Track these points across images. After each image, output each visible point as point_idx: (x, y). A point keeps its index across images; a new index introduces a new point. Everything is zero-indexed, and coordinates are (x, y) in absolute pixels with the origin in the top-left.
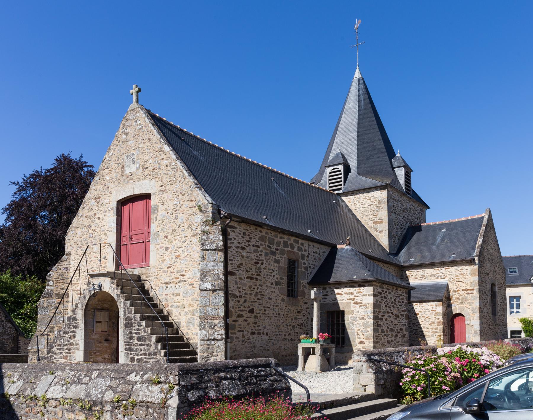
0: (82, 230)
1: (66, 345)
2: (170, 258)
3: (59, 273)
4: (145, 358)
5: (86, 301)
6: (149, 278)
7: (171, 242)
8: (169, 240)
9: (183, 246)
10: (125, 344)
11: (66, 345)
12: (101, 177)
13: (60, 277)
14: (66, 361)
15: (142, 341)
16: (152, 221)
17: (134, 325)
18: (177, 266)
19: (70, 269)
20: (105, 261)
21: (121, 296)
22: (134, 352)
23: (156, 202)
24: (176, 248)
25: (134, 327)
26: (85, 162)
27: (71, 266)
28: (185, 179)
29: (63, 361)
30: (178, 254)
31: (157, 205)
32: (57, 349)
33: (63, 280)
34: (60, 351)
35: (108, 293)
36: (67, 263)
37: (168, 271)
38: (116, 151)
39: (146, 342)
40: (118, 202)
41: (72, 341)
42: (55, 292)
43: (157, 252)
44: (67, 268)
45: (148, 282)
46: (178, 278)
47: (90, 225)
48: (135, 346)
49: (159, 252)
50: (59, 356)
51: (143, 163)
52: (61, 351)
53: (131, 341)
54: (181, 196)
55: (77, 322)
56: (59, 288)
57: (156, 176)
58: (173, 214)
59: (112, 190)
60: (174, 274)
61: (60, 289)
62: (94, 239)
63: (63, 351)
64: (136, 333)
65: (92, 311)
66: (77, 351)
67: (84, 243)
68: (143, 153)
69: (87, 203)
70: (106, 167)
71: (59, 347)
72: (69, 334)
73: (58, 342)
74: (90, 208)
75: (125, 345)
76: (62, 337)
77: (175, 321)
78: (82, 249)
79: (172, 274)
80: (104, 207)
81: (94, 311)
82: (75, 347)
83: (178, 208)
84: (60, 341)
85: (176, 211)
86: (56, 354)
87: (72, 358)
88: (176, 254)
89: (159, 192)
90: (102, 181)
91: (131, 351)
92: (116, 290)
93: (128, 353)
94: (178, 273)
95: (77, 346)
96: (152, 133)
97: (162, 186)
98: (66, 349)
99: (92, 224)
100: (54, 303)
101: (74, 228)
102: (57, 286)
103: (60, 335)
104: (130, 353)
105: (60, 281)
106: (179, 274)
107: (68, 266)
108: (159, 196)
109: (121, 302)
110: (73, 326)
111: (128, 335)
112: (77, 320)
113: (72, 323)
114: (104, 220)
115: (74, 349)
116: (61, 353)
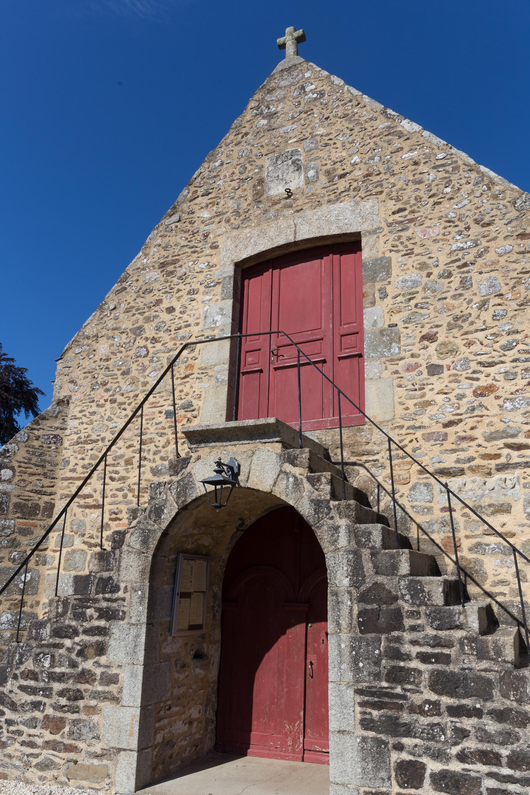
0: (111, 342)
1: (61, 678)
2: (452, 396)
3: (33, 447)
4: (490, 775)
5: (164, 526)
6: (364, 458)
7: (453, 351)
8: (444, 344)
9: (508, 359)
10: (359, 699)
11: (61, 678)
12: (185, 216)
13: (34, 459)
14: (58, 737)
15: (466, 696)
16: (366, 301)
17: (408, 622)
18: (486, 420)
19: (65, 439)
20: (189, 415)
21: (338, 507)
22: (417, 741)
23: (382, 250)
24: (474, 366)
25: (413, 628)
26: (5, 354)
27: (68, 432)
28: (491, 183)
29: (40, 736)
30: (484, 382)
31: (384, 258)
32: (22, 688)
33: (43, 467)
34: (30, 698)
35: (269, 495)
36: (57, 423)
37: (446, 435)
38: (235, 155)
39: (489, 697)
40: (237, 265)
41: (88, 665)
42: (15, 500)
43: (396, 382)
44: (55, 436)
45: (362, 471)
46: (498, 456)
47: (140, 328)
48: (422, 712)
49: (404, 382)
50: (28, 716)
51: (329, 167)
52: (39, 698)
53: (398, 690)
54: (476, 230)
55: (115, 596)
56: (28, 488)
57: (379, 189)
58: (450, 275)
59: (221, 241)
60: (474, 444)
61: (31, 491)
62: (151, 361)
63: (45, 700)
64: (424, 658)
65: (173, 557)
66: (106, 706)
67: (116, 372)
68: (326, 145)
69: (135, 278)
70: (199, 193)
71: (32, 683)
72: (77, 639)
73: (29, 665)
74: (144, 288)
75: (362, 704)
76: (48, 646)
77: (499, 599)
78: (108, 386)
79: (464, 445)
80: (188, 280)
81: (176, 560)
82: (100, 688)
83: (469, 258)
84: (37, 660)
85: (465, 265)
86: (13, 707)
87: (85, 731)
88: (476, 384)
89: (390, 225)
90: (187, 224)
91: (396, 734)
92: (307, 485)
93: (379, 742)
94: (495, 439)
95: (113, 688)
96: (355, 103)
97: (400, 210)
98: (61, 694)
99: (146, 326)
100: (8, 531)
101: (88, 338)
102: (22, 484)
103: (38, 638)
104: (392, 741)
105: (34, 470)
106: (500, 443)
107: (58, 432)
108: (392, 237)
109: (337, 528)
110: (98, 610)
111: (377, 663)
112: (116, 589)
113: (96, 601)
114: (188, 312)
115: (96, 695)
116: (36, 705)
